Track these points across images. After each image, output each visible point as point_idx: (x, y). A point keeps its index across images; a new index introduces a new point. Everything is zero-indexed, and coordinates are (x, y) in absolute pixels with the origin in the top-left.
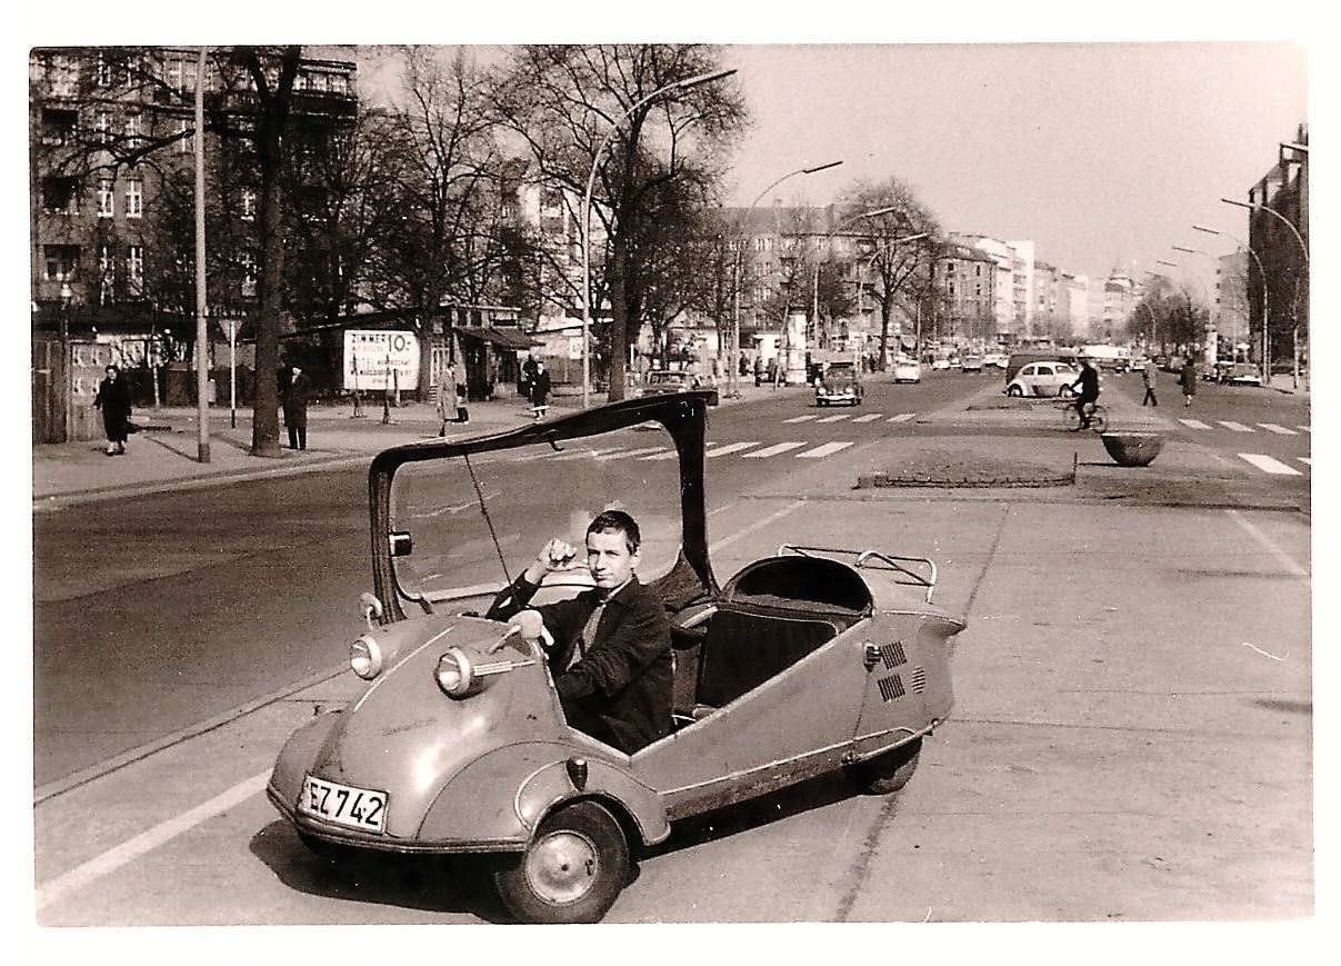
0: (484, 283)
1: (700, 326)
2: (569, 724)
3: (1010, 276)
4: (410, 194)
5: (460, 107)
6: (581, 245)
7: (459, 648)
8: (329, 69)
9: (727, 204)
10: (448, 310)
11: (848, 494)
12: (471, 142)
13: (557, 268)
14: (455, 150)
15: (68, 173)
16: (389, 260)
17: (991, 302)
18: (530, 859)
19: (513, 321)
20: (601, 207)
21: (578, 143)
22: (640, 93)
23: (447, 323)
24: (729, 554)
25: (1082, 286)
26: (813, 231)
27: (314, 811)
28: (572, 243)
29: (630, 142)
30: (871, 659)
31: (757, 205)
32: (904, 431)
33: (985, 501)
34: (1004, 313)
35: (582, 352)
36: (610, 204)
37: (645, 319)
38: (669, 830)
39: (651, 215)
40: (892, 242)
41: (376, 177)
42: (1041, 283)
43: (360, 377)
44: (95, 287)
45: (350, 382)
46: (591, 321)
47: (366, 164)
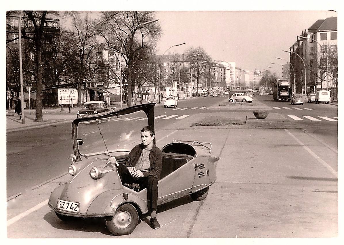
0: (94, 76)
1: (150, 86)
4: (74, 53)
8: (52, 21)
9: (157, 54)
10: (85, 83)
12: (90, 39)
13: (113, 71)
16: (69, 70)
17: (225, 78)
20: (124, 55)
23: (85, 86)
25: (247, 73)
27: (61, 208)
28: (117, 65)
29: (131, 39)
34: (228, 81)
36: (127, 55)
40: (199, 63)
42: (237, 73)
43: (62, 100)
45: (60, 102)
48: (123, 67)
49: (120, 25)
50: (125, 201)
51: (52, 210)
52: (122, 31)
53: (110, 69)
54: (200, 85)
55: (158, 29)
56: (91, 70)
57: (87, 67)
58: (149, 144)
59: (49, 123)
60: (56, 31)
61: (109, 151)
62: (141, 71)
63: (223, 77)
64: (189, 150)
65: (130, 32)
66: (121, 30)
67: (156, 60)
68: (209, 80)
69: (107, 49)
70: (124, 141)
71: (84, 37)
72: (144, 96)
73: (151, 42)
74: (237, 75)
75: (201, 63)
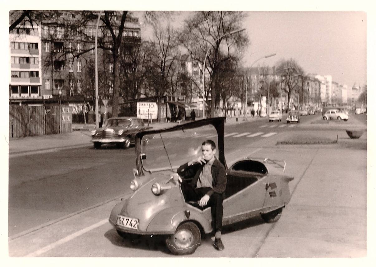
1: (237, 101)
3: (325, 86)
4: (156, 65)
10: (166, 97)
15: (60, 60)
16: (149, 83)
17: (320, 93)
23: (165, 100)
24: (231, 161)
25: (345, 88)
29: (216, 49)
34: (323, 96)
36: (211, 67)
44: (69, 91)
47: (143, 57)
49: (204, 34)
57: (169, 80)
60: (137, 40)
64: (260, 168)
66: (205, 40)
67: (243, 72)
68: (301, 95)
71: (165, 48)
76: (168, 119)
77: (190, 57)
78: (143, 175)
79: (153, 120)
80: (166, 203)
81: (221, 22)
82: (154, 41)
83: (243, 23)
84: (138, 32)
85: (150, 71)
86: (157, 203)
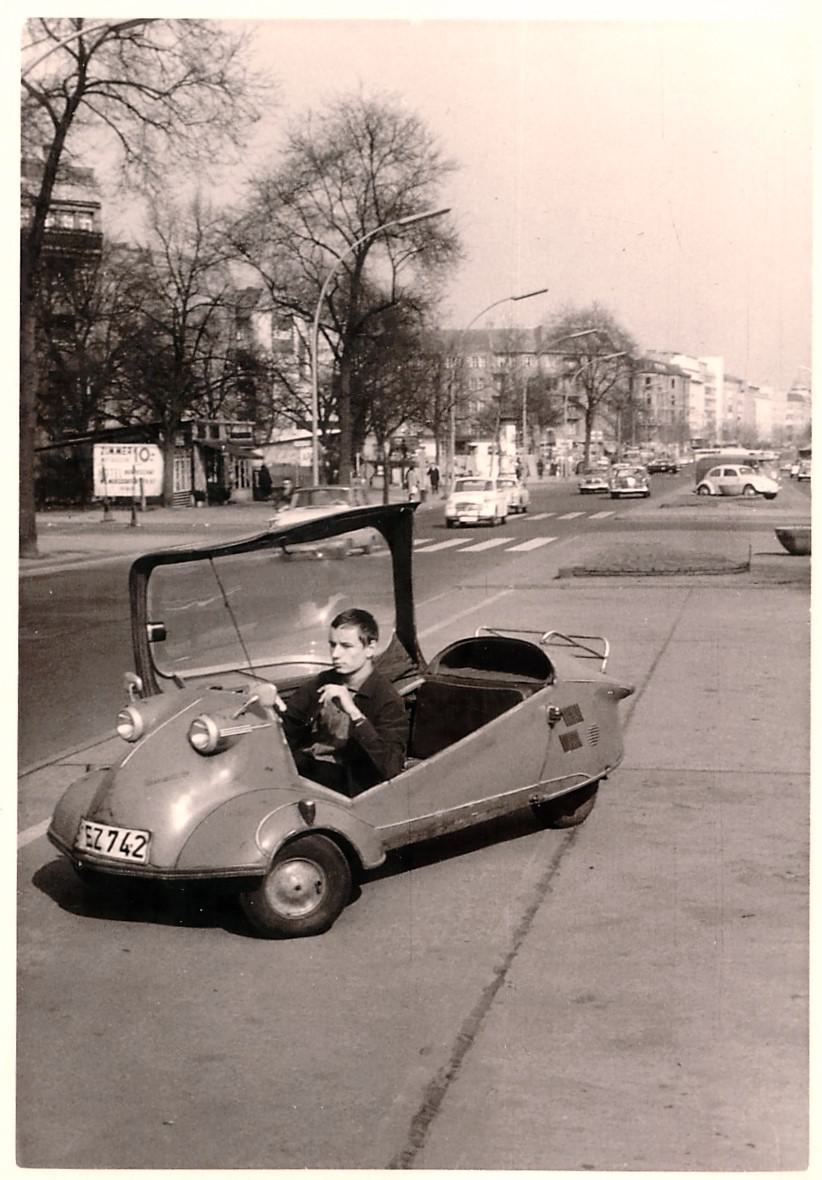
0: (221, 400)
2: (300, 774)
4: (155, 324)
5: (198, 245)
6: (310, 366)
7: (209, 715)
8: (75, 208)
9: (443, 328)
10: (188, 424)
11: (549, 582)
12: (208, 275)
13: (288, 385)
14: (194, 282)
16: (133, 379)
17: (685, 413)
18: (268, 883)
19: (249, 434)
20: (327, 331)
21: (306, 275)
22: (364, 230)
23: (188, 437)
24: (436, 635)
25: (765, 396)
26: (524, 350)
27: (88, 849)
28: (302, 363)
29: (354, 273)
30: (553, 719)
31: (473, 327)
32: (603, 527)
33: (669, 587)
34: (697, 422)
35: (312, 460)
36: (337, 329)
37: (370, 430)
38: (384, 857)
39: (374, 338)
40: (595, 359)
41: (120, 305)
42: (730, 394)
43: (109, 485)
45: (101, 490)
46: (319, 432)
48: (322, 371)
50: (304, 825)
51: (61, 854)
52: (323, 248)
53: (276, 378)
54: (596, 435)
55: (448, 240)
56: (213, 380)
57: (198, 370)
58: (574, 581)
59: (62, 563)
61: (255, 663)
62: (386, 383)
63: (678, 409)
64: (530, 662)
65: (348, 249)
67: (442, 347)
69: (267, 308)
70: (304, 629)
71: (185, 268)
72: (396, 473)
73: (423, 287)
74: (730, 403)
75: (601, 358)
76: (199, 496)
77: (266, 298)
78: (159, 691)
79: (148, 498)
80: (237, 778)
81: (371, 186)
82: (149, 246)
83: (442, 191)
84: (92, 214)
85: (136, 341)
86: (207, 778)
